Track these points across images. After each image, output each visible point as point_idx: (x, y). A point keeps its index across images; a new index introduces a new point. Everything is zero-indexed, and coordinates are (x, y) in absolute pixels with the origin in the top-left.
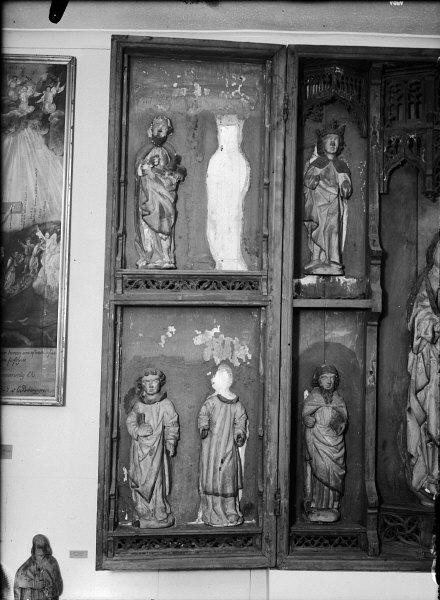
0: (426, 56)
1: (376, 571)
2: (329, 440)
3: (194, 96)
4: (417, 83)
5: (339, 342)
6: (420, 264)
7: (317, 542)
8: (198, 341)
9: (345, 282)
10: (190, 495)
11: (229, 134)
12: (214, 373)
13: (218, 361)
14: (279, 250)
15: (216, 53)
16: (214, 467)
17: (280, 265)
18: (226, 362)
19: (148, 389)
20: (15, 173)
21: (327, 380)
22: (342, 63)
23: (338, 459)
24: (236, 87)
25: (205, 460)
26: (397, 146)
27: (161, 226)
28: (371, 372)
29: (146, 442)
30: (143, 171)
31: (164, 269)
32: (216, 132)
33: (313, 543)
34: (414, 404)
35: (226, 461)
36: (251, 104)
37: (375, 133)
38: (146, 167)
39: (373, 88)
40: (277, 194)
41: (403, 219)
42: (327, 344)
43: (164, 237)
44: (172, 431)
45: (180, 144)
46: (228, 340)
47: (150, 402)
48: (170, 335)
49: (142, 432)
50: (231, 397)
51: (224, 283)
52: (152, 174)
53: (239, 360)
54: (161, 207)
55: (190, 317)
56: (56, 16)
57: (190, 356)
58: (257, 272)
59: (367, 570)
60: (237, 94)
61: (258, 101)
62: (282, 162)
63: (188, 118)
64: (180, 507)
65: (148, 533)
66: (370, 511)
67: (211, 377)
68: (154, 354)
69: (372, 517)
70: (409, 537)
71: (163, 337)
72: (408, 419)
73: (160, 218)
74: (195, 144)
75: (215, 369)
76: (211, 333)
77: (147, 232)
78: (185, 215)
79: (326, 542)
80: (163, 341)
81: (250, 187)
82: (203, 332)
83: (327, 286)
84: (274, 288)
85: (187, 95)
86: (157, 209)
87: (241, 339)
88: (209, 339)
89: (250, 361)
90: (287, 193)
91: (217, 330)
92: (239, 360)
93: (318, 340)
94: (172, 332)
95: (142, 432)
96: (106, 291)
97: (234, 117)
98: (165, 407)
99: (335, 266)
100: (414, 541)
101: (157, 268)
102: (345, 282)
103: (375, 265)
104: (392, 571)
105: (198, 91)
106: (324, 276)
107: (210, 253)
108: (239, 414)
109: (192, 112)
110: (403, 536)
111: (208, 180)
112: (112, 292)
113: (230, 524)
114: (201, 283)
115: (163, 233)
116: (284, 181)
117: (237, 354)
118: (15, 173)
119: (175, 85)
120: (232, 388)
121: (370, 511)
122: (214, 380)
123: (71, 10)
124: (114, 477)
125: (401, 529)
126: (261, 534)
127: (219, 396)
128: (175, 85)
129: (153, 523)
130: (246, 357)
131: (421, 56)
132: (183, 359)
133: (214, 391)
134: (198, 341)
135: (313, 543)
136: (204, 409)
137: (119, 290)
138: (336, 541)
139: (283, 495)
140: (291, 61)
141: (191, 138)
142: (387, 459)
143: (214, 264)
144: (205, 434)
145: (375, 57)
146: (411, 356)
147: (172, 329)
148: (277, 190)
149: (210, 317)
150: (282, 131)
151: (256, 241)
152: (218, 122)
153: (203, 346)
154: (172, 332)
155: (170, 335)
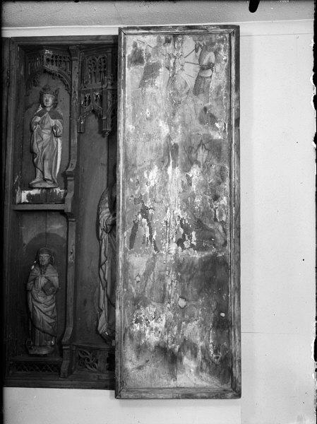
1: (65, 388)
5: (56, 232)
9: (60, 192)
21: (45, 257)
22: (50, 47)
26: (89, 101)
28: (72, 253)
37: (75, 92)
39: (73, 62)
42: (47, 234)
56: (253, 8)
59: (59, 388)
83: (47, 195)
93: (41, 232)
102: (60, 192)
103: (71, 180)
104: (75, 388)
106: (46, 188)
123: (261, 6)
124: (70, 315)
125: (88, 360)
142: (86, 312)
145: (71, 42)
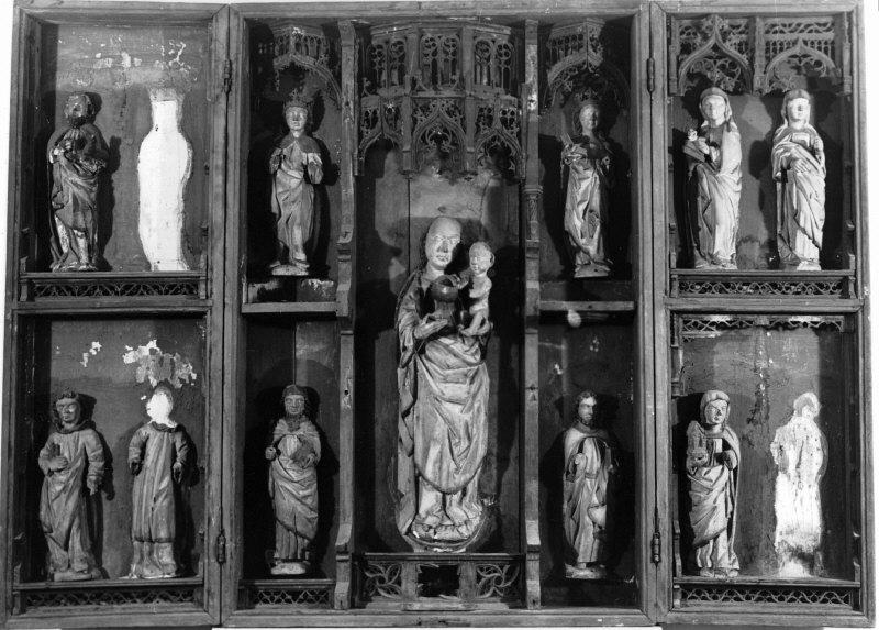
0: (399, 10)
2: (293, 475)
3: (123, 69)
4: (432, 39)
6: (412, 261)
7: (276, 597)
8: (129, 358)
10: (121, 544)
11: (165, 112)
12: (149, 397)
13: (154, 382)
14: (220, 246)
15: (140, 17)
16: (146, 508)
17: (222, 264)
18: (164, 384)
19: (64, 415)
20: (752, 578)
23: (305, 497)
24: (174, 56)
25: (136, 499)
27: (75, 221)
28: (346, 392)
29: (62, 477)
30: (55, 157)
31: (82, 271)
32: (150, 109)
33: (272, 599)
34: (403, 432)
35: (160, 499)
36: (193, 75)
37: (347, 104)
38: (56, 152)
40: (218, 179)
41: (391, 207)
43: (80, 234)
44: (96, 466)
45: (108, 125)
46: (168, 356)
47: (68, 432)
48: (94, 353)
49: (54, 465)
50: (172, 425)
51: (156, 287)
52: (63, 161)
53: (182, 381)
54: (75, 198)
55: (118, 328)
57: (121, 377)
58: (195, 273)
60: (175, 63)
61: (202, 71)
62: (223, 141)
63: (114, 94)
64: (110, 559)
65: (62, 585)
66: (339, 557)
67: (146, 401)
68: (74, 375)
69: (342, 565)
70: (390, 590)
71: (85, 355)
72: (399, 451)
73: (74, 211)
74: (123, 124)
75: (151, 391)
76: (145, 350)
77: (61, 230)
78: (108, 209)
79: (289, 597)
80: (86, 360)
81: (192, 173)
82: (135, 349)
84: (215, 291)
85: (114, 67)
86: (71, 201)
87: (183, 356)
88: (141, 355)
89: (194, 381)
90: (231, 178)
91: (153, 344)
92: (182, 381)
94: (96, 349)
95: (54, 465)
96: (9, 299)
97: (172, 92)
98: (88, 437)
99: (300, 265)
100: (397, 593)
101: (71, 270)
102: (320, 286)
105: (127, 62)
107: (143, 255)
108: (178, 445)
109: (119, 86)
110: (383, 589)
111: (140, 167)
112: (15, 300)
113: (167, 576)
114: (127, 288)
115: (79, 230)
116: (226, 163)
117: (179, 373)
118: (752, 578)
119: (98, 55)
120: (172, 416)
121: (339, 557)
122: (149, 405)
126: (203, 585)
127: (154, 425)
128: (98, 55)
129: (69, 575)
130: (190, 377)
131: (393, 10)
132: (110, 380)
133: (149, 418)
134: (129, 358)
135: (272, 599)
136: (135, 440)
137: (24, 297)
138: (301, 597)
139: (228, 536)
140: (234, 22)
141: (118, 117)
143: (148, 266)
144: (137, 467)
146: (400, 371)
147: (96, 345)
148: (217, 175)
149: (146, 327)
150: (223, 105)
151: (195, 238)
152: (152, 97)
153: (136, 365)
154: (96, 349)
155: (94, 353)
